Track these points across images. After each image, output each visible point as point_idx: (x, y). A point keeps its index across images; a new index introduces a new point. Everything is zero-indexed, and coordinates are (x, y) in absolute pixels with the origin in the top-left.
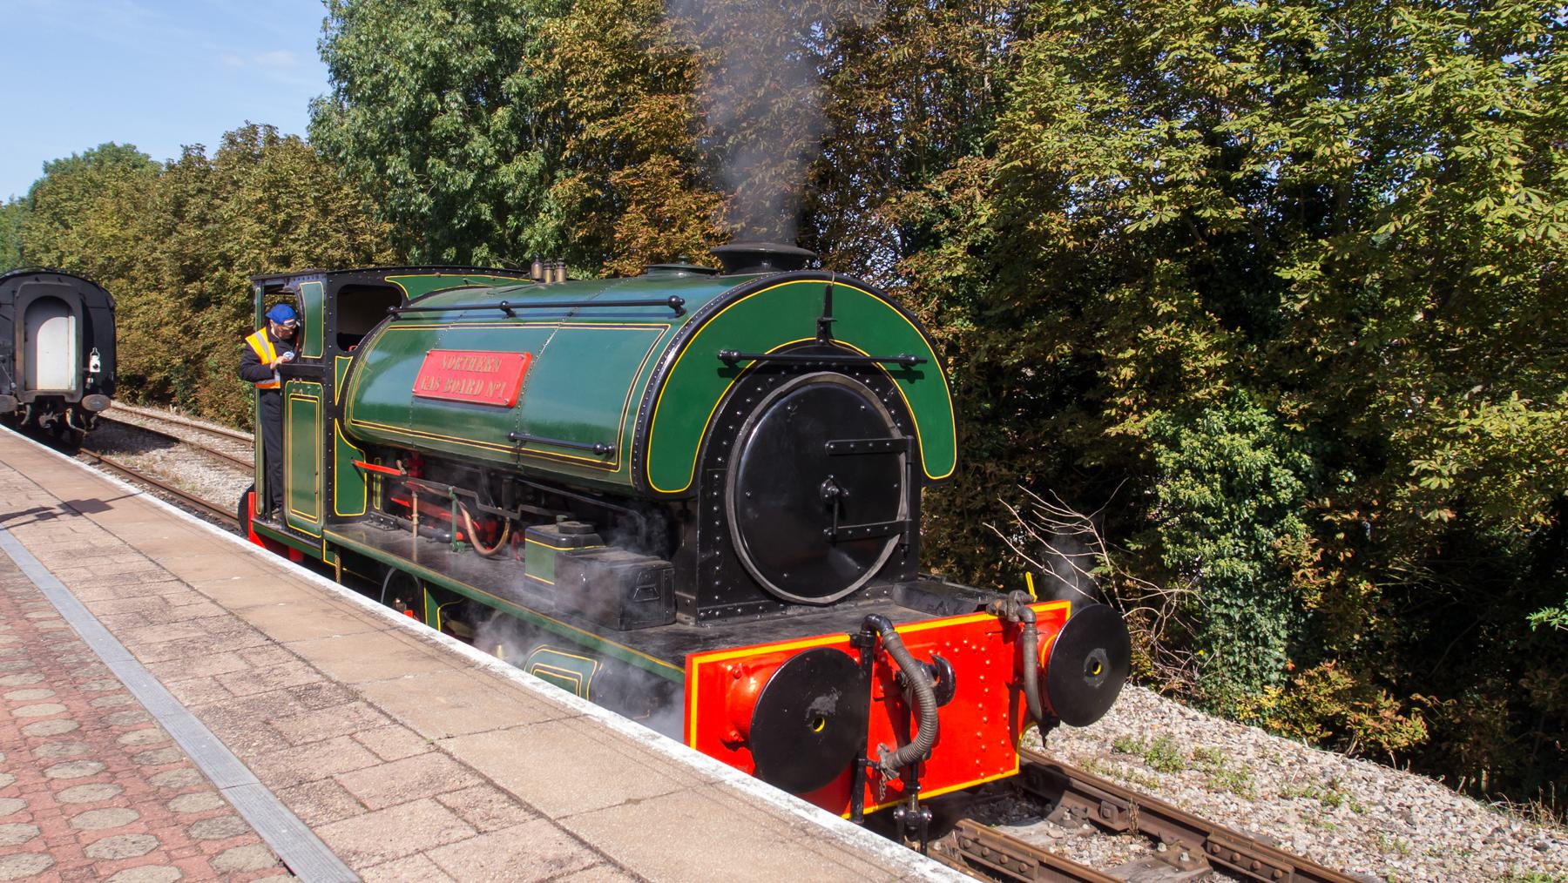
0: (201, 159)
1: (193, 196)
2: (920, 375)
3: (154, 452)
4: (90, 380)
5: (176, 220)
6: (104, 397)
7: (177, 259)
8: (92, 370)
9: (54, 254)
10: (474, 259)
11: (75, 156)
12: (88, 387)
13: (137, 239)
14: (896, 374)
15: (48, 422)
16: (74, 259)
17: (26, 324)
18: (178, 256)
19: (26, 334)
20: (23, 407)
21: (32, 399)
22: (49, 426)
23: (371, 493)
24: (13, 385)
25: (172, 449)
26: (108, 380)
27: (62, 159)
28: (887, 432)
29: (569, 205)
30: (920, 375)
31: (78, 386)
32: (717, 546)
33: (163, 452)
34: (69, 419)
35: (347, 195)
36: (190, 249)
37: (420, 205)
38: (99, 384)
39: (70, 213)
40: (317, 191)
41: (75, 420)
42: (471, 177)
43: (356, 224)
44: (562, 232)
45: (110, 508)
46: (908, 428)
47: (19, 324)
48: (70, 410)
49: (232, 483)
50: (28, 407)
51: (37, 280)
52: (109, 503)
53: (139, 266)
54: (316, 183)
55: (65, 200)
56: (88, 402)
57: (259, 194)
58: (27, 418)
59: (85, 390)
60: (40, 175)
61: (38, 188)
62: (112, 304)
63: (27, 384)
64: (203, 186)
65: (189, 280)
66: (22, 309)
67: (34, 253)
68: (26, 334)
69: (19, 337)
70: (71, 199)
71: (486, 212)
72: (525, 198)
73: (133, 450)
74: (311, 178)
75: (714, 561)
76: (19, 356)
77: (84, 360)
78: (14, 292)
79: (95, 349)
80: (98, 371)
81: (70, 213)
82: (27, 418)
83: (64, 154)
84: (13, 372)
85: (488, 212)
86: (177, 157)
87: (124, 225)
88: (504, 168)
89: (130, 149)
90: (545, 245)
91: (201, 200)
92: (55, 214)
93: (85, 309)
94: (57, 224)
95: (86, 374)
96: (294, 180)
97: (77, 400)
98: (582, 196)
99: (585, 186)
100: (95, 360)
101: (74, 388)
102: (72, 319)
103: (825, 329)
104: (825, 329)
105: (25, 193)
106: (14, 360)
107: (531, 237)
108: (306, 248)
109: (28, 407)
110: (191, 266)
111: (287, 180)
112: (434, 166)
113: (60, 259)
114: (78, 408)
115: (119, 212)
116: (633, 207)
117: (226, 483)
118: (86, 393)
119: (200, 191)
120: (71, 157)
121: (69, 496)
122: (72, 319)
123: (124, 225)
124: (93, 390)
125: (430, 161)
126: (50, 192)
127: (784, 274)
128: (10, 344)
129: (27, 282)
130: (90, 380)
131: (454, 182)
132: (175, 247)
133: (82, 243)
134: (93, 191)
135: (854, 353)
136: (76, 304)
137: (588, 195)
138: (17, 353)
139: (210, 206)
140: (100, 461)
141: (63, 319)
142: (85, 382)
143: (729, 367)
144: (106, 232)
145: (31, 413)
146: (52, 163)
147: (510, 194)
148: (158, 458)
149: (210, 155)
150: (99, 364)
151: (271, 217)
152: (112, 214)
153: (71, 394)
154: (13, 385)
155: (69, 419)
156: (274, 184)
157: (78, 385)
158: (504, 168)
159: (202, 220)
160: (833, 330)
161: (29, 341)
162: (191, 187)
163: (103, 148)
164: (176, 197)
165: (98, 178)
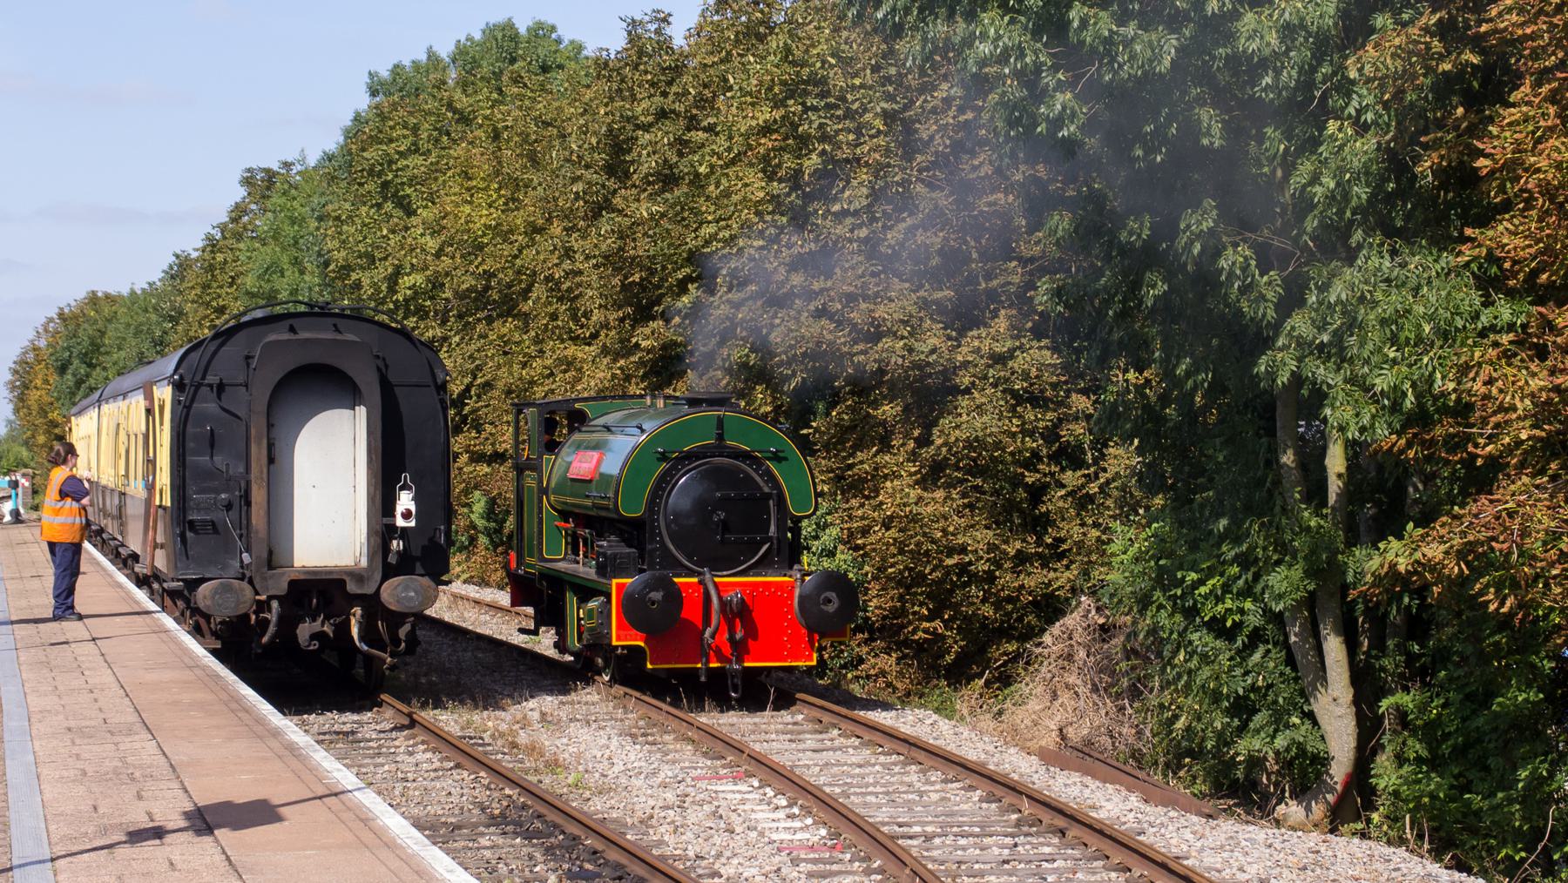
0: (664, 45)
1: (646, 128)
2: (785, 459)
3: (532, 703)
4: (397, 545)
5: (611, 184)
6: (426, 581)
7: (618, 270)
8: (400, 522)
9: (383, 270)
10: (1183, 240)
11: (431, 55)
12: (392, 559)
13: (534, 230)
14: (769, 459)
15: (314, 637)
16: (418, 279)
17: (270, 426)
18: (614, 261)
19: (270, 446)
20: (262, 606)
21: (282, 587)
22: (315, 645)
23: (567, 543)
24: (246, 557)
25: (573, 696)
26: (433, 541)
27: (407, 62)
28: (760, 488)
29: (1399, 94)
30: (785, 459)
31: (371, 558)
32: (658, 542)
33: (548, 702)
34: (355, 631)
35: (947, 101)
36: (642, 247)
37: (1058, 123)
38: (417, 552)
39: (412, 181)
40: (890, 98)
41: (368, 633)
42: (1170, 46)
43: (975, 168)
44: (1396, 162)
45: (279, 819)
46: (777, 485)
47: (258, 426)
48: (358, 610)
49: (667, 772)
50: (275, 604)
51: (292, 330)
52: (283, 811)
53: (539, 291)
54: (888, 80)
55: (402, 155)
56: (397, 593)
57: (765, 114)
58: (272, 629)
59: (386, 565)
60: (363, 102)
61: (361, 134)
62: (440, 376)
63: (274, 555)
64: (668, 103)
65: (644, 314)
66: (261, 395)
67: (347, 269)
68: (270, 446)
69: (258, 453)
70: (415, 150)
71: (1212, 127)
72: (1306, 84)
73: (488, 699)
74: (876, 69)
75: (656, 549)
76: (258, 495)
77: (383, 502)
78: (248, 358)
79: (406, 477)
80: (413, 524)
81: (412, 181)
82: (272, 629)
83: (411, 53)
84: (245, 526)
85: (1216, 128)
86: (614, 41)
87: (513, 203)
88: (1249, 18)
89: (542, 32)
90: (1346, 197)
91: (662, 136)
92: (385, 185)
93: (387, 388)
94: (389, 206)
95: (389, 531)
96: (838, 81)
97: (369, 589)
98: (1429, 70)
99: (1437, 45)
100: (405, 501)
101: (364, 563)
102: (361, 411)
103: (720, 437)
104: (720, 437)
105: (331, 141)
106: (248, 504)
107: (1315, 179)
108: (863, 233)
109: (275, 604)
110: (641, 284)
111: (824, 81)
112: (1084, 23)
113: (393, 280)
114: (372, 604)
115: (497, 173)
116: (1526, 89)
117: (655, 773)
118: (389, 572)
119: (662, 114)
120: (423, 57)
121: (210, 792)
122: (361, 411)
123: (513, 203)
124: (404, 566)
125: (1075, 14)
126: (374, 140)
127: (692, 410)
128: (241, 469)
129: (279, 335)
130: (397, 545)
131: (1133, 57)
132: (610, 243)
133: (432, 244)
134: (457, 129)
135: (739, 448)
136: (368, 381)
137: (1447, 66)
138: (254, 488)
139: (681, 146)
140: (413, 723)
141: (345, 413)
142: (386, 549)
143: (663, 457)
144: (483, 217)
145: (281, 618)
146: (385, 74)
147: (1268, 80)
148: (536, 715)
149: (678, 35)
150: (413, 509)
151: (789, 162)
152: (487, 179)
153: (358, 576)
154: (246, 557)
155: (355, 631)
156: (793, 90)
157: (371, 557)
158: (1249, 18)
159: (667, 179)
160: (726, 437)
161: (277, 461)
162: (643, 108)
163: (490, 31)
164: (610, 130)
165: (462, 101)
